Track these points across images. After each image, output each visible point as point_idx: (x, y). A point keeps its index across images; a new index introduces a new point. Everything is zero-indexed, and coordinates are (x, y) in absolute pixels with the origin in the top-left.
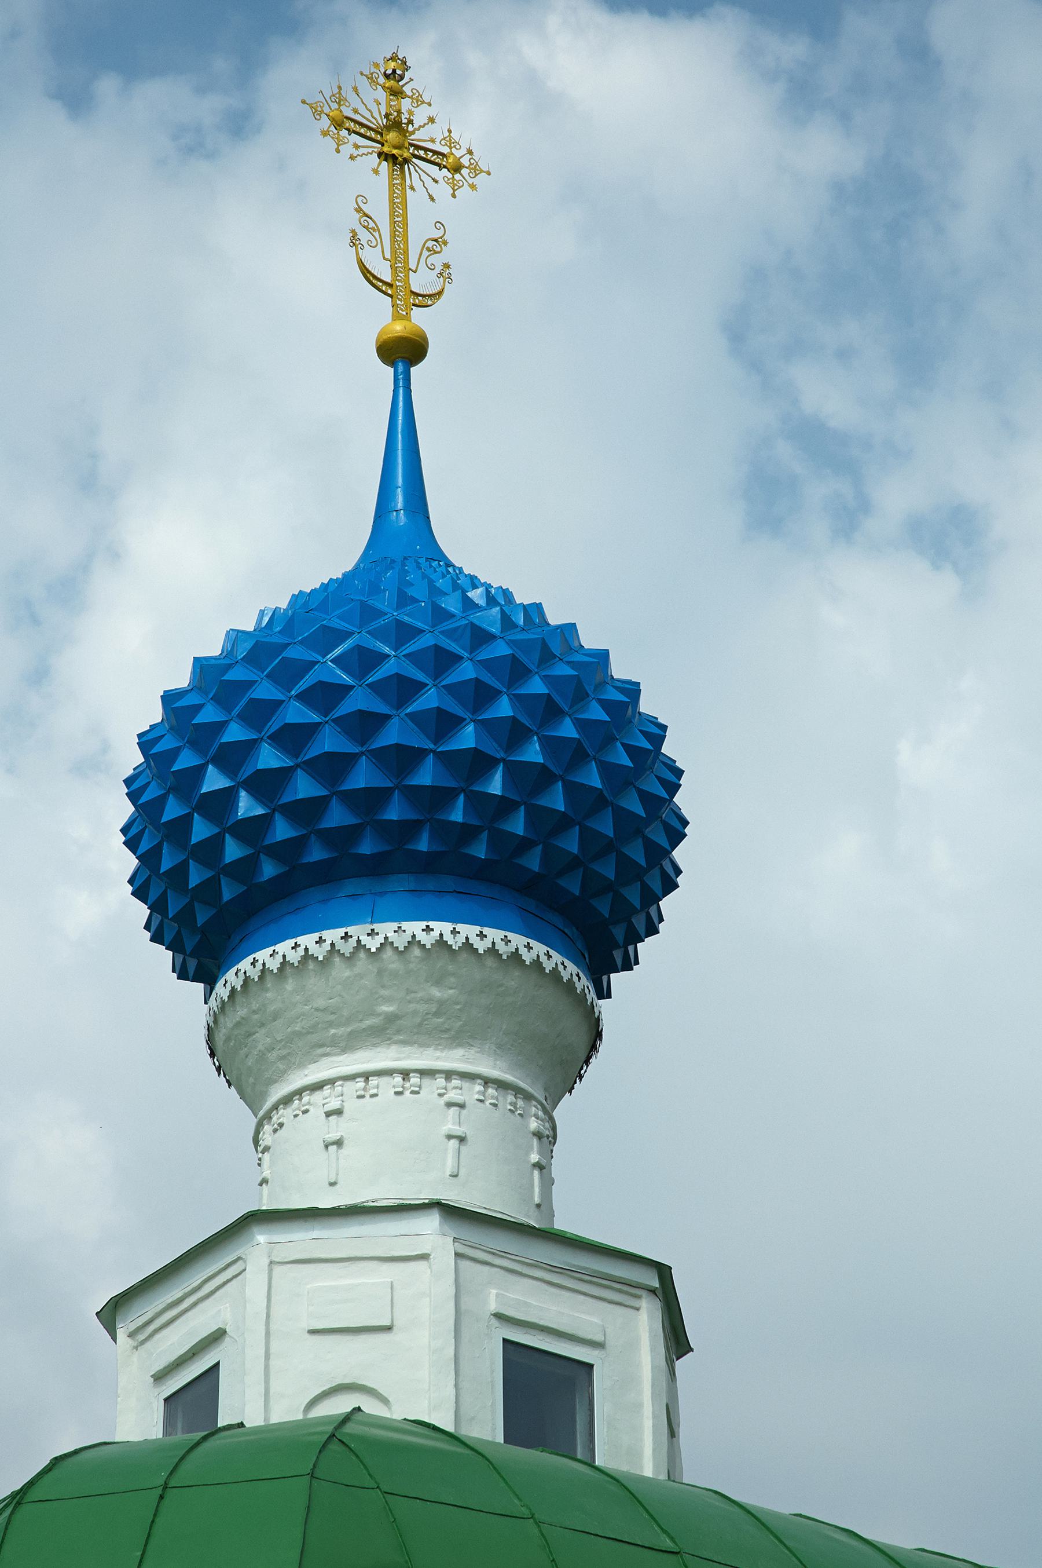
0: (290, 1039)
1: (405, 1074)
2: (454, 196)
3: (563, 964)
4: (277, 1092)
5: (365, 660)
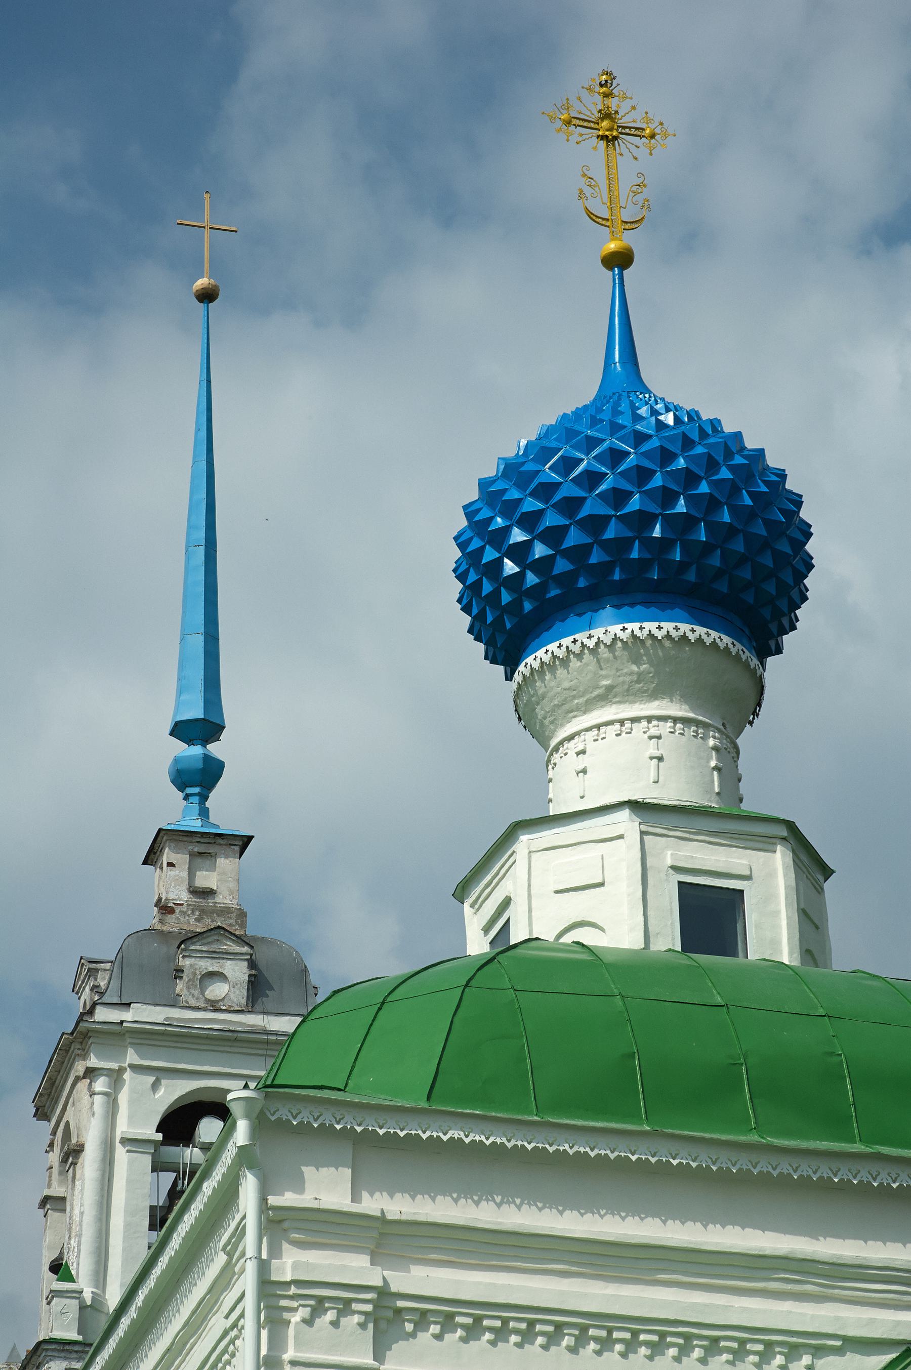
0: (553, 710)
1: (622, 722)
2: (651, 154)
3: (720, 638)
4: (553, 743)
5: (568, 464)
